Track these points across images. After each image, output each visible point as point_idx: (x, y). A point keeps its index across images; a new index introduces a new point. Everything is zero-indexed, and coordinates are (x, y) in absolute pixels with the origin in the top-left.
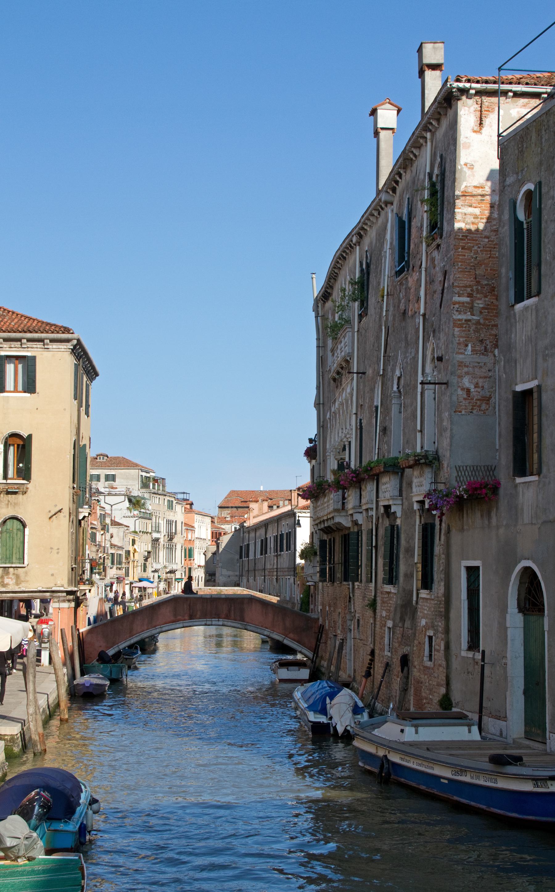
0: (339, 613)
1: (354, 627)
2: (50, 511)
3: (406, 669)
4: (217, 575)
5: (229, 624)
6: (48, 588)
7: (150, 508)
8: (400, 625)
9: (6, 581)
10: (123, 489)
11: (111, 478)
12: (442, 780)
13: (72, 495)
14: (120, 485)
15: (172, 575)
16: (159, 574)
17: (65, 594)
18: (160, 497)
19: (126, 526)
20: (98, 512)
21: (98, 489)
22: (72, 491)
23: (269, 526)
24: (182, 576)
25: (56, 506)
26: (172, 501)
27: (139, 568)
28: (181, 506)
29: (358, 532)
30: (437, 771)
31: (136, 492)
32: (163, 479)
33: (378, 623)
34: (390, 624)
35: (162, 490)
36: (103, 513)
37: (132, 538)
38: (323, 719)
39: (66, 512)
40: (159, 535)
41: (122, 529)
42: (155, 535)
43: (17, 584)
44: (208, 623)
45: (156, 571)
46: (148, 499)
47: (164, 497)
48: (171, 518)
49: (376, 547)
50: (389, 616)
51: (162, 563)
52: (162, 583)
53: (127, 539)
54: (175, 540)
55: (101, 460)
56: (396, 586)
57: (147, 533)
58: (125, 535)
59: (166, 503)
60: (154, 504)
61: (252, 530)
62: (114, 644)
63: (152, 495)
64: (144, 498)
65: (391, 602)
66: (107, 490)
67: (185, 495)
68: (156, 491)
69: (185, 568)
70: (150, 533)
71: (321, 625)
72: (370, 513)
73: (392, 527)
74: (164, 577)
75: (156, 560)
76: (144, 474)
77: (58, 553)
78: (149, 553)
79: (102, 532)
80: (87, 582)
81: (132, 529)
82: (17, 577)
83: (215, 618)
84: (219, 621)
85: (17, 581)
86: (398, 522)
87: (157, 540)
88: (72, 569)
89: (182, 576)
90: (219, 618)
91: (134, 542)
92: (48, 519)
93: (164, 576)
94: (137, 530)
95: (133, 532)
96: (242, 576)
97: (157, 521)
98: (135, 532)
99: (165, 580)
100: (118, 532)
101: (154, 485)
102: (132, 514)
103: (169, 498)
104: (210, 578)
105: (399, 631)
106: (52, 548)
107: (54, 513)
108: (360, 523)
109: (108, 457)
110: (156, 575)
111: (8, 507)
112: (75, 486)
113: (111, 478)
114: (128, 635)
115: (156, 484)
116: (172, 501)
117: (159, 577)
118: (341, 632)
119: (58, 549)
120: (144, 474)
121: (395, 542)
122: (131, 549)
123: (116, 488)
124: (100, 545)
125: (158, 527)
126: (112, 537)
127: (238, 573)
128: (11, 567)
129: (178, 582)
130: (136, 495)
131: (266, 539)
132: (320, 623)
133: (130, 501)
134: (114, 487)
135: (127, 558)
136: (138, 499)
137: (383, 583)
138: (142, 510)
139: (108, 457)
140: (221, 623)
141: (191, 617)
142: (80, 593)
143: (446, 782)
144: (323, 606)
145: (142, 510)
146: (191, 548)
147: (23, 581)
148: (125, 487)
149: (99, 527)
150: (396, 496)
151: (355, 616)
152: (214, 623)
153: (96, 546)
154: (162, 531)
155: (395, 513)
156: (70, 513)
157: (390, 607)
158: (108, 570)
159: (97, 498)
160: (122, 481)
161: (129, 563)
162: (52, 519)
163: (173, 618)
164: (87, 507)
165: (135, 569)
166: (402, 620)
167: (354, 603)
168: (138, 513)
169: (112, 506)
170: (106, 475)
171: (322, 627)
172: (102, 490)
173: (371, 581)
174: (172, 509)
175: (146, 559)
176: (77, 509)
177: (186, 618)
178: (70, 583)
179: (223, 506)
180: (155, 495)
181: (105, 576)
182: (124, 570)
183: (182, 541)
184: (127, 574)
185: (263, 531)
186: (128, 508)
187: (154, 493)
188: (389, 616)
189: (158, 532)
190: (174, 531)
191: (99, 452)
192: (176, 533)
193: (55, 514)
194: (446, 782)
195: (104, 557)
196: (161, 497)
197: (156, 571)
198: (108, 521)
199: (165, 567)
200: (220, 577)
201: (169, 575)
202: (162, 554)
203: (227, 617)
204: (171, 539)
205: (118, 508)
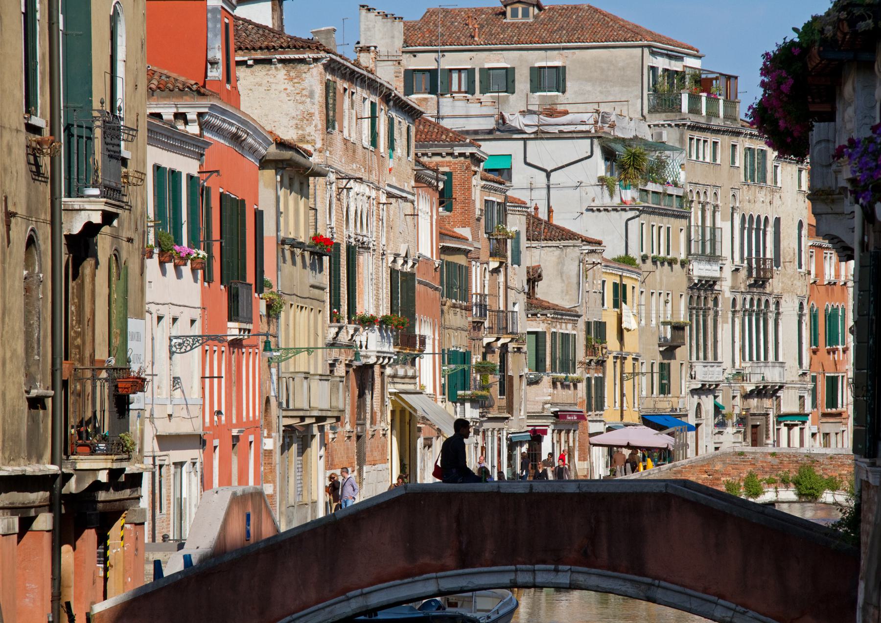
7: (682, 177)
10: (585, 117)
14: (579, 102)
15: (767, 403)
16: (720, 400)
18: (719, 138)
19: (589, 242)
20: (478, 197)
21: (502, 117)
27: (644, 381)
31: (633, 122)
32: (729, 77)
35: (726, 117)
36: (497, 198)
37: (610, 281)
41: (574, 253)
42: (701, 270)
44: (522, 578)
45: (704, 390)
46: (673, 149)
47: (734, 140)
48: (759, 209)
51: (727, 364)
52: (730, 430)
53: (592, 285)
54: (775, 285)
55: (520, 19)
57: (671, 262)
58: (584, 270)
59: (739, 161)
63: (688, 134)
64: (660, 146)
66: (533, 120)
68: (702, 120)
69: (814, 379)
70: (683, 264)
74: (737, 411)
75: (707, 350)
76: (662, 63)
78: (678, 328)
79: (494, 264)
80: (102, 446)
81: (613, 249)
83: (544, 562)
84: (557, 571)
87: (708, 285)
90: (558, 561)
91: (620, 294)
93: (737, 406)
94: (635, 253)
95: (618, 260)
97: (708, 223)
98: (626, 261)
99: (742, 421)
100: (561, 262)
101: (694, 99)
102: (617, 201)
103: (748, 143)
109: (540, 8)
110: (708, 403)
113: (550, 79)
115: (704, 95)
116: (763, 153)
117: (717, 409)
120: (662, 63)
122: (609, 318)
123: (566, 113)
124: (482, 307)
125: (713, 240)
129: (790, 427)
130: (629, 135)
133: (609, 155)
134: (560, 108)
135: (591, 349)
136: (636, 148)
138: (651, 187)
139: (540, 8)
142: (78, 482)
146: (835, 310)
148: (591, 107)
149: (483, 244)
152: (540, 578)
153: (468, 309)
154: (726, 252)
159: (468, 151)
160: (588, 87)
161: (601, 363)
163: (402, 564)
164: (96, 192)
165: (628, 384)
168: (636, 195)
170: (532, 69)
172: (516, 121)
174: (764, 179)
175: (669, 351)
177: (449, 561)
180: (697, 135)
181: (510, 408)
182: (582, 386)
183: (802, 287)
184: (596, 400)
186: (601, 180)
187: (695, 127)
189: (713, 258)
190: (770, 254)
192: (777, 261)
195: (505, 346)
196: (724, 141)
197: (704, 390)
198: (516, 224)
199: (740, 376)
201: (754, 402)
202: (727, 334)
204: (760, 282)
205: (563, 180)
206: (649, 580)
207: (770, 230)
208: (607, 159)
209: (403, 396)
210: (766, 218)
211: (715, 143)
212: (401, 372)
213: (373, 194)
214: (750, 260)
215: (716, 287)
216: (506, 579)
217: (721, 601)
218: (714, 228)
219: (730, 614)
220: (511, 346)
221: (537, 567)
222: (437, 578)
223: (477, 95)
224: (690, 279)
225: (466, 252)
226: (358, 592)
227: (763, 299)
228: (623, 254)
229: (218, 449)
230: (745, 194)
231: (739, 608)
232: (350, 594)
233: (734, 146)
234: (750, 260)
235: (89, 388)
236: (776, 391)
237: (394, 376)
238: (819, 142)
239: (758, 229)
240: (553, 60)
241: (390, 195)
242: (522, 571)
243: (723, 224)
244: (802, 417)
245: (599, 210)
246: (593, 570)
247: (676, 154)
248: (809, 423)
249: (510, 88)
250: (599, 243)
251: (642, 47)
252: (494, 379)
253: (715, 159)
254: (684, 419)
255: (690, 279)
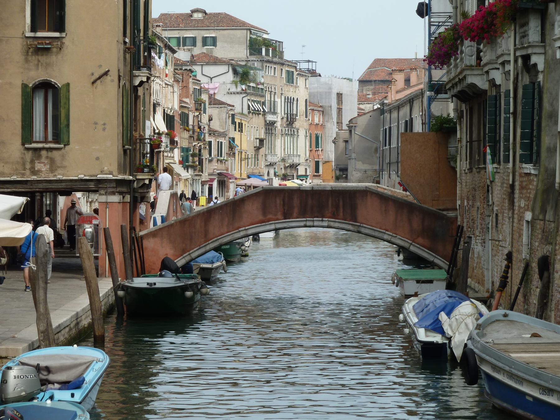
0: (478, 208)
1: (492, 225)
2: (93, 74)
3: (546, 274)
4: (349, 170)
5: (337, 225)
6: (91, 176)
8: (541, 217)
9: (38, 166)
11: (209, 41)
12: (528, 398)
13: (122, 52)
17: (114, 185)
22: (122, 47)
23: (415, 102)
24: (306, 172)
25: (100, 66)
26: (293, 72)
28: (304, 78)
29: (496, 96)
30: (525, 389)
33: (516, 216)
34: (528, 216)
38: (437, 338)
39: (114, 75)
40: (275, 117)
42: (270, 118)
43: (52, 169)
44: (308, 223)
45: (271, 165)
46: (259, 70)
48: (291, 94)
49: (515, 114)
50: (528, 205)
54: (297, 124)
56: (538, 165)
59: (284, 75)
60: (268, 76)
61: (394, 108)
62: (184, 251)
65: (531, 187)
67: (310, 64)
71: (459, 226)
72: (507, 67)
73: (533, 83)
75: (272, 149)
77: (104, 129)
78: (261, 141)
79: (197, 114)
82: (52, 161)
84: (322, 221)
85: (51, 166)
86: (541, 78)
87: (273, 123)
88: (125, 151)
89: (306, 172)
90: (323, 217)
92: (90, 85)
95: (239, 113)
96: (382, 170)
97: (272, 99)
104: (341, 173)
105: (539, 224)
106: (96, 123)
107: (98, 77)
108: (498, 82)
111: (38, 69)
112: (127, 40)
114: (203, 240)
116: (293, 72)
118: (480, 233)
119: (104, 124)
121: (536, 105)
126: (210, 120)
127: (377, 167)
128: (43, 148)
131: (411, 119)
132: (459, 223)
133: (235, 72)
137: (521, 161)
138: (252, 84)
140: (325, 224)
141: (287, 215)
143: (531, 399)
144: (461, 201)
145: (252, 84)
147: (59, 167)
150: (537, 42)
151: (493, 209)
152: (316, 223)
154: (279, 111)
155: (535, 65)
156: (119, 76)
157: (530, 193)
158: (205, 164)
159: (188, 68)
162: (95, 85)
163: (261, 217)
166: (544, 211)
167: (492, 194)
169: (211, 79)
171: (460, 229)
173: (509, 162)
174: (293, 83)
176: (131, 71)
177: (279, 216)
178: (122, 169)
179: (365, 80)
185: (407, 109)
188: (528, 205)
189: (275, 113)
190: (295, 112)
191: (193, 8)
192: (297, 115)
193: (99, 78)
194: (531, 399)
195: (200, 146)
199: (283, 160)
200: (354, 173)
203: (334, 216)
206: (359, 224)
207: (295, 102)
208: (234, 74)
209: (171, 164)
210: (294, 98)
211: (275, 68)
212: (169, 155)
213: (161, 83)
214: (287, 114)
215: (275, 125)
216: (302, 224)
217: (387, 232)
218: (274, 102)
219: (390, 237)
220: (202, 146)
221: (315, 219)
222: (275, 223)
223: (181, 47)
224: (265, 121)
225: (188, 108)
226: (244, 228)
227: (292, 130)
228: (241, 112)
229: (462, 133)
230: (285, 88)
231: (394, 235)
232: (240, 229)
233: (282, 69)
234: (287, 114)
235: (138, 147)
236: (297, 166)
237: (167, 156)
238: (468, 47)
239: (290, 102)
240: (212, 34)
241: (166, 84)
242: (309, 221)
243: (278, 100)
244: (306, 176)
245: (234, 93)
246: (337, 220)
247: (261, 72)
248: (308, 179)
249: (194, 45)
250: (233, 106)
251: (247, 29)
252: (196, 159)
253: (275, 74)
254: (263, 177)
255: (265, 121)
